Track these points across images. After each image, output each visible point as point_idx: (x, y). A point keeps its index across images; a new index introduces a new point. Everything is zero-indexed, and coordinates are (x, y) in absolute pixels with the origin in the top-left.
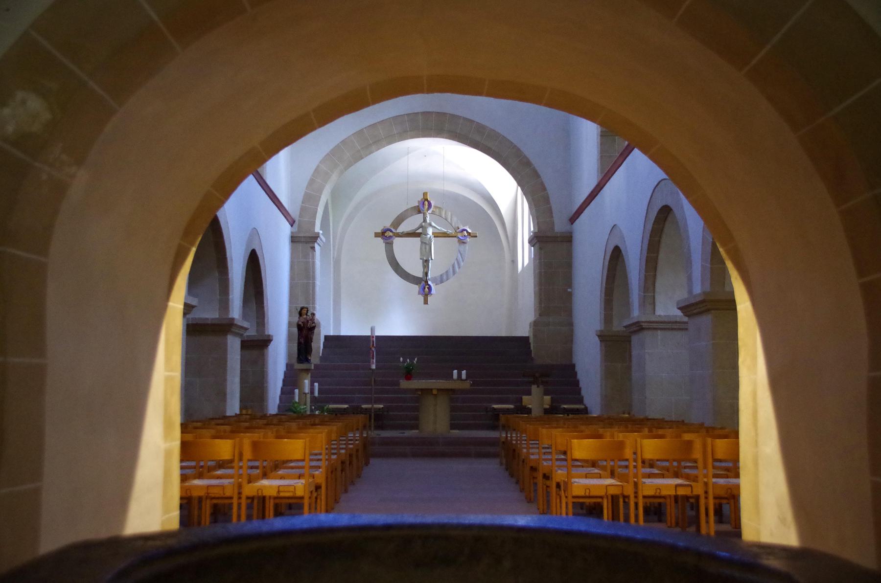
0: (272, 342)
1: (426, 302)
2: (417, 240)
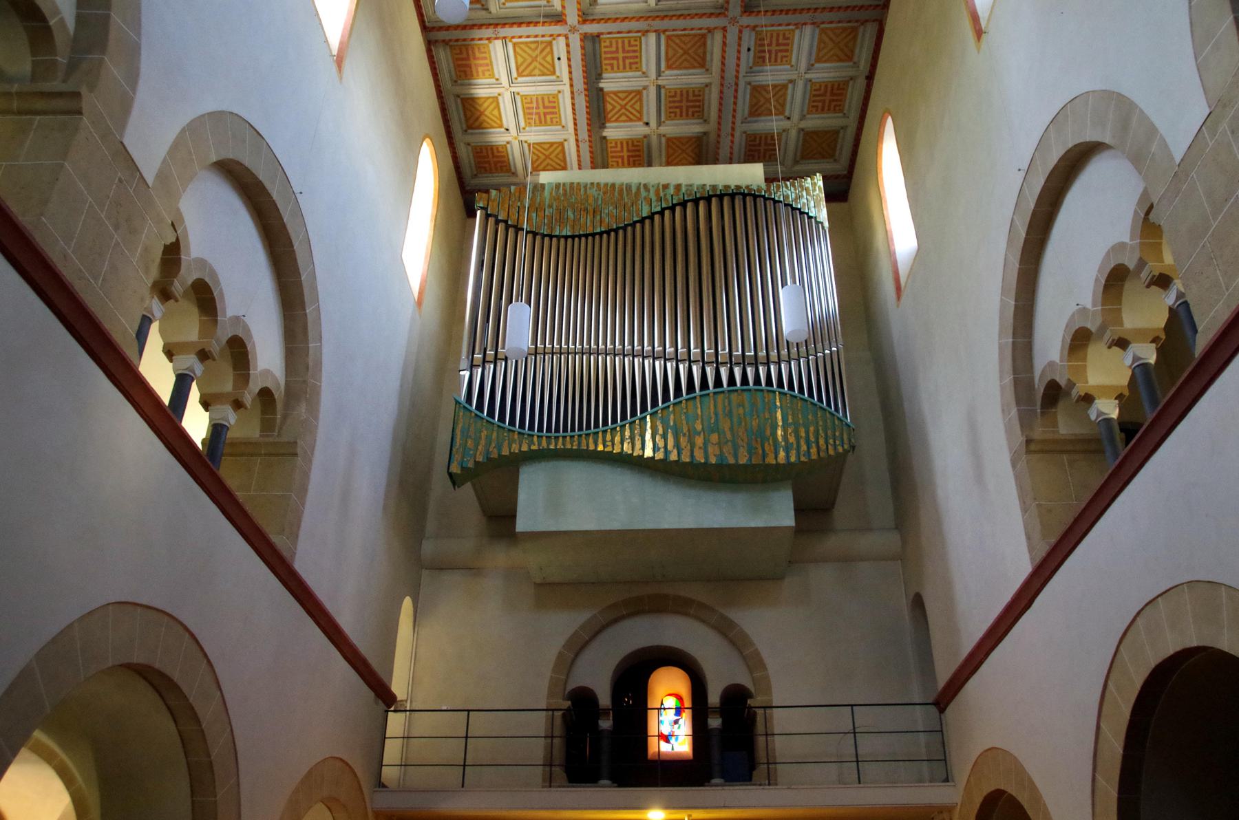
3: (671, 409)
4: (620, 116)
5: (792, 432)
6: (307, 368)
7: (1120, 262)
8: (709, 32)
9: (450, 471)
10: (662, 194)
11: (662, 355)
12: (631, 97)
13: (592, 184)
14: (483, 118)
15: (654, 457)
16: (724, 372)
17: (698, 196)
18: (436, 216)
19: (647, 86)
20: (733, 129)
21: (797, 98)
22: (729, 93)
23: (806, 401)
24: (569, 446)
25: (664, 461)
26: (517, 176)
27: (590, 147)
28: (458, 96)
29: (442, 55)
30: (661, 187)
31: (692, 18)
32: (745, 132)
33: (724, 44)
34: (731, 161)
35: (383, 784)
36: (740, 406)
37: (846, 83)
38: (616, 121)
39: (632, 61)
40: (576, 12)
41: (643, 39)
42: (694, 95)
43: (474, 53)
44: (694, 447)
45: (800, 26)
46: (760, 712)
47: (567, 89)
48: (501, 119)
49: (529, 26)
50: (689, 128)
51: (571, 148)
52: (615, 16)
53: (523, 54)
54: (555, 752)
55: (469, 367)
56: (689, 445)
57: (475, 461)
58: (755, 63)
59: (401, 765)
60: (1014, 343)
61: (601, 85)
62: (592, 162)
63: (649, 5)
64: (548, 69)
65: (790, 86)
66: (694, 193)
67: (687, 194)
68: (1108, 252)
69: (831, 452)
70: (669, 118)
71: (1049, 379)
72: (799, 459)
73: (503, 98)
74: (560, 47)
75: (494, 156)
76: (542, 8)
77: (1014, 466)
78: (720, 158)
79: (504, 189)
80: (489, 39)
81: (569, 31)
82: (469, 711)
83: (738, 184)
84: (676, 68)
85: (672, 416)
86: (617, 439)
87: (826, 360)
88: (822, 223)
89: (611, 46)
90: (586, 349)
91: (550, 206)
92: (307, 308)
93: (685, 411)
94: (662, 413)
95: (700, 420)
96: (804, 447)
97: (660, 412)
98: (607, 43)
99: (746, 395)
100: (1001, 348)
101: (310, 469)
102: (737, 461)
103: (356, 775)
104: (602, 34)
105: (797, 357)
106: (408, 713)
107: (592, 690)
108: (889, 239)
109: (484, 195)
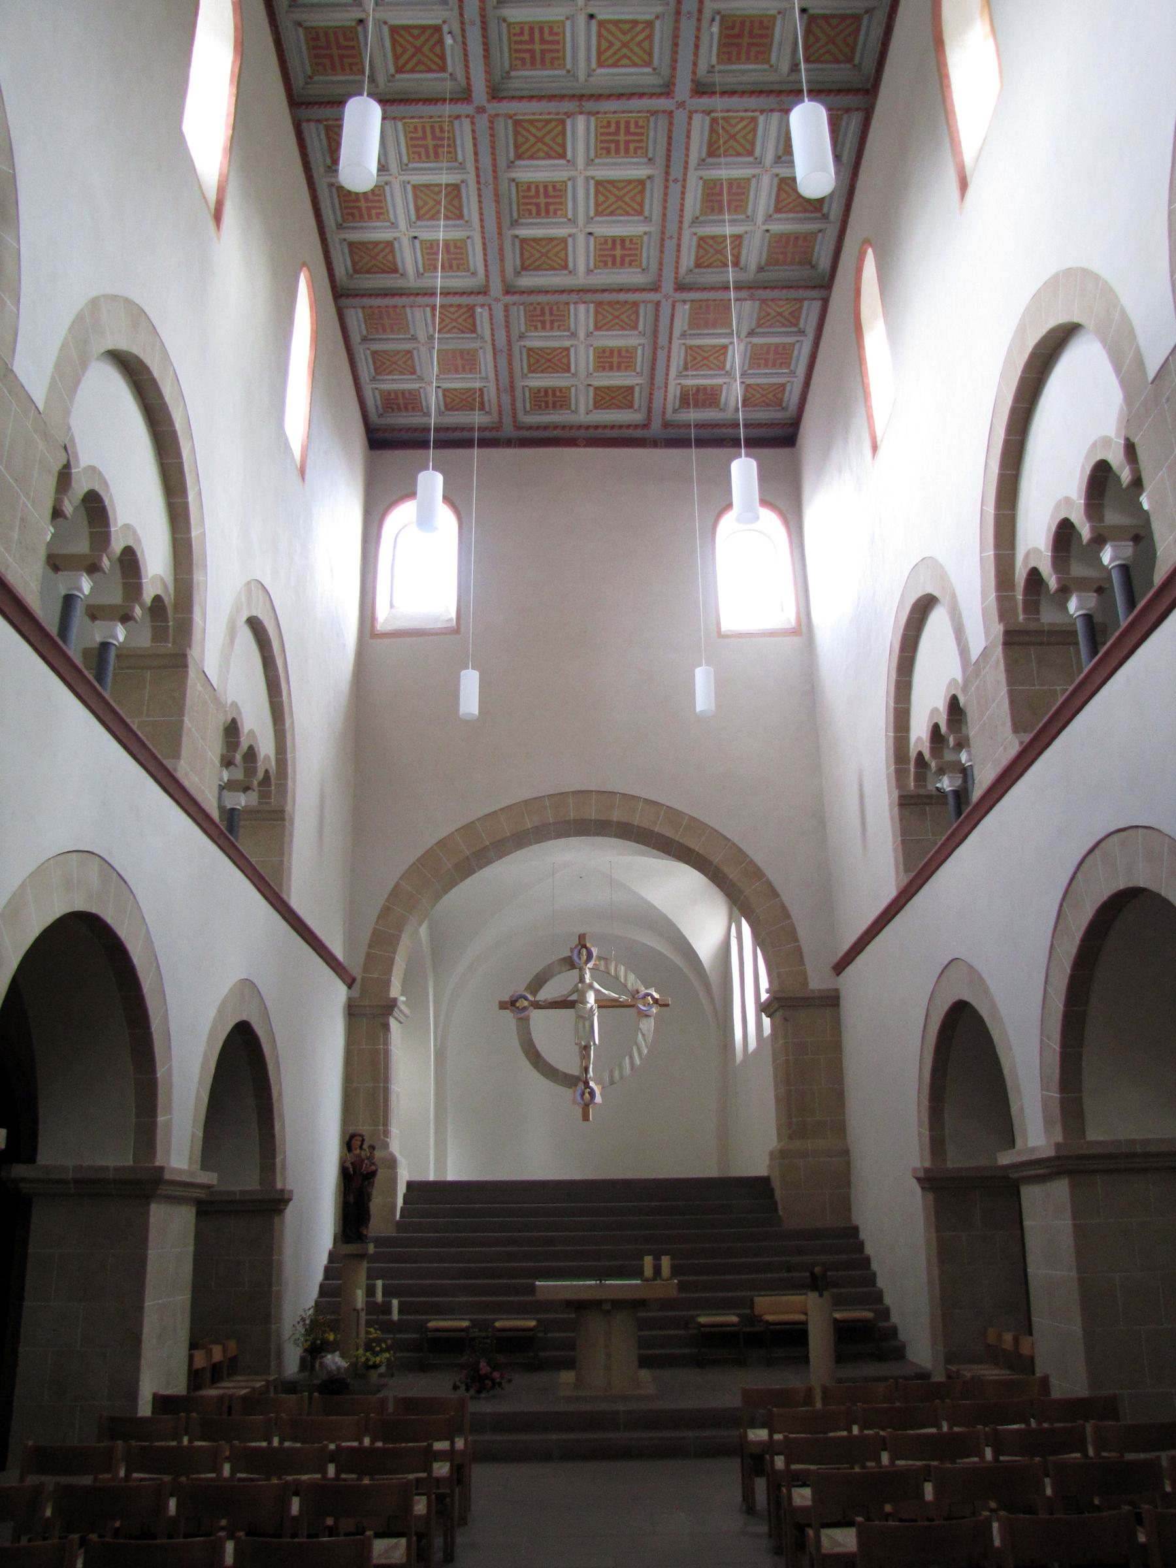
0: (291, 1204)
1: (586, 1117)
2: (568, 1013)
31: (629, 99)
47: (471, 178)
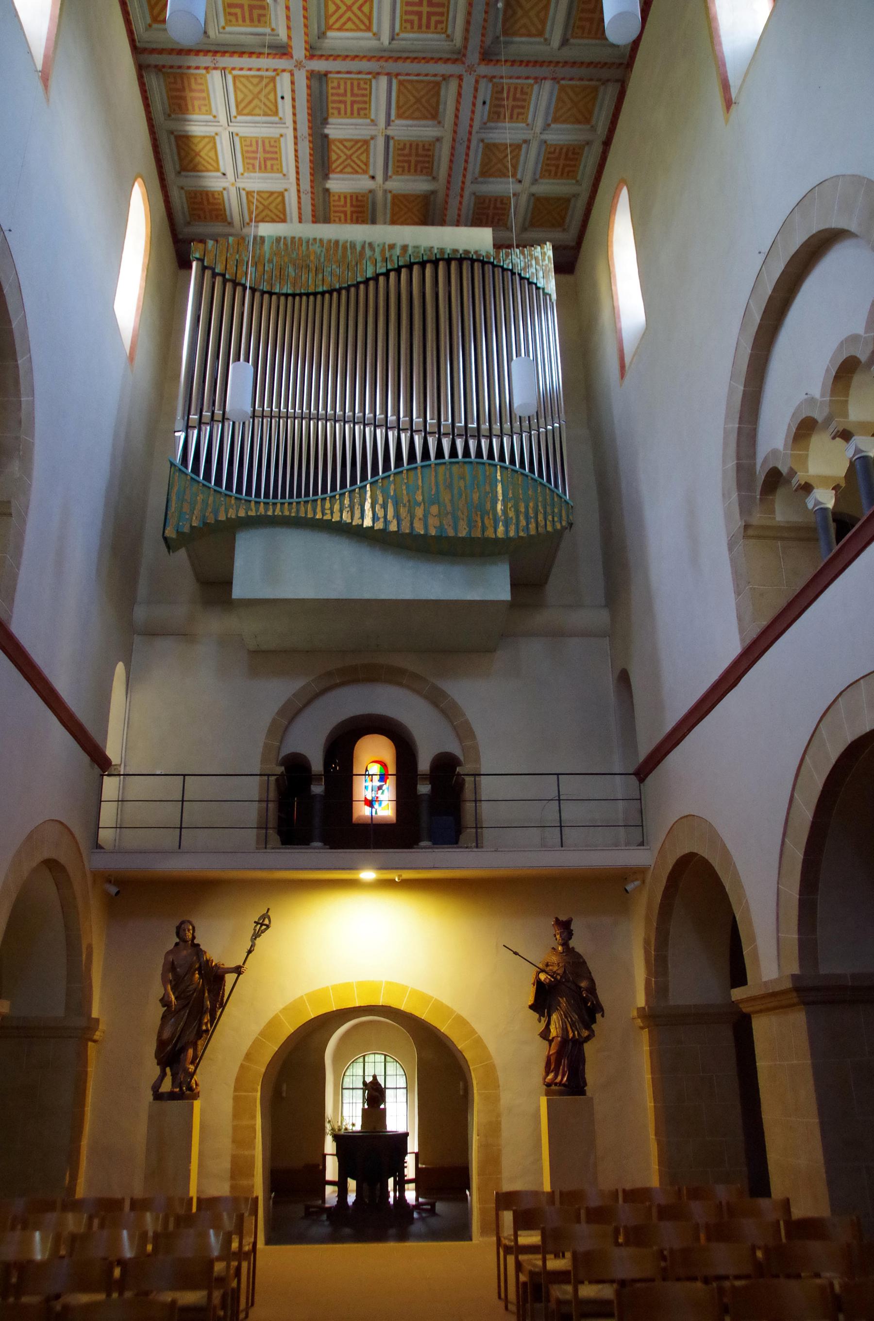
3: (392, 478)
4: (345, 167)
5: (512, 506)
6: (20, 422)
7: (853, 354)
8: (444, 79)
9: (165, 536)
10: (387, 255)
11: (362, 420)
12: (357, 147)
13: (315, 239)
14: (198, 159)
15: (373, 527)
16: (446, 443)
17: (425, 258)
18: (148, 265)
19: (376, 136)
20: (462, 189)
21: (531, 158)
22: (461, 149)
23: (527, 476)
24: (287, 513)
25: (384, 531)
26: (233, 226)
27: (313, 199)
28: (172, 133)
29: (155, 82)
30: (387, 247)
31: (428, 62)
32: (474, 194)
33: (459, 94)
34: (458, 224)
35: (100, 845)
36: (461, 478)
37: (582, 147)
38: (341, 172)
39: (361, 106)
40: (303, 45)
41: (374, 82)
42: (424, 149)
43: (189, 84)
44: (414, 518)
45: (539, 81)
46: (469, 780)
48: (217, 162)
49: (242, 57)
50: (417, 185)
51: (292, 199)
52: (346, 54)
53: (244, 89)
54: (270, 813)
55: (185, 427)
56: (409, 515)
57: (191, 525)
58: (490, 119)
59: (116, 828)
60: (739, 428)
61: (326, 131)
62: (313, 216)
63: (382, 44)
64: (270, 109)
65: (524, 146)
66: (434, 254)
67: (414, 256)
68: (842, 342)
69: (549, 529)
70: (396, 173)
71: (771, 466)
72: (518, 532)
73: (221, 137)
74: (284, 84)
75: (209, 203)
76: (267, 37)
77: (730, 549)
78: (448, 218)
79: (222, 240)
80: (206, 68)
81: (295, 66)
82: (184, 775)
83: (467, 248)
84: (407, 118)
85: (392, 486)
86: (337, 507)
87: (548, 436)
88: (550, 295)
89: (339, 87)
90: (305, 413)
91: (270, 261)
92: (18, 358)
93: (406, 481)
94: (382, 482)
95: (420, 491)
96: (523, 523)
97: (380, 481)
98: (335, 84)
99: (467, 468)
100: (726, 433)
101: (24, 531)
102: (456, 534)
103: (74, 837)
104: (330, 72)
105: (519, 432)
106: (122, 777)
107: (305, 757)
108: (616, 316)
109: (201, 246)
